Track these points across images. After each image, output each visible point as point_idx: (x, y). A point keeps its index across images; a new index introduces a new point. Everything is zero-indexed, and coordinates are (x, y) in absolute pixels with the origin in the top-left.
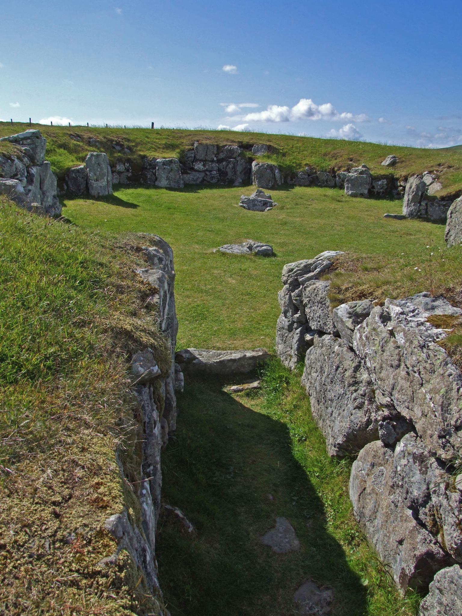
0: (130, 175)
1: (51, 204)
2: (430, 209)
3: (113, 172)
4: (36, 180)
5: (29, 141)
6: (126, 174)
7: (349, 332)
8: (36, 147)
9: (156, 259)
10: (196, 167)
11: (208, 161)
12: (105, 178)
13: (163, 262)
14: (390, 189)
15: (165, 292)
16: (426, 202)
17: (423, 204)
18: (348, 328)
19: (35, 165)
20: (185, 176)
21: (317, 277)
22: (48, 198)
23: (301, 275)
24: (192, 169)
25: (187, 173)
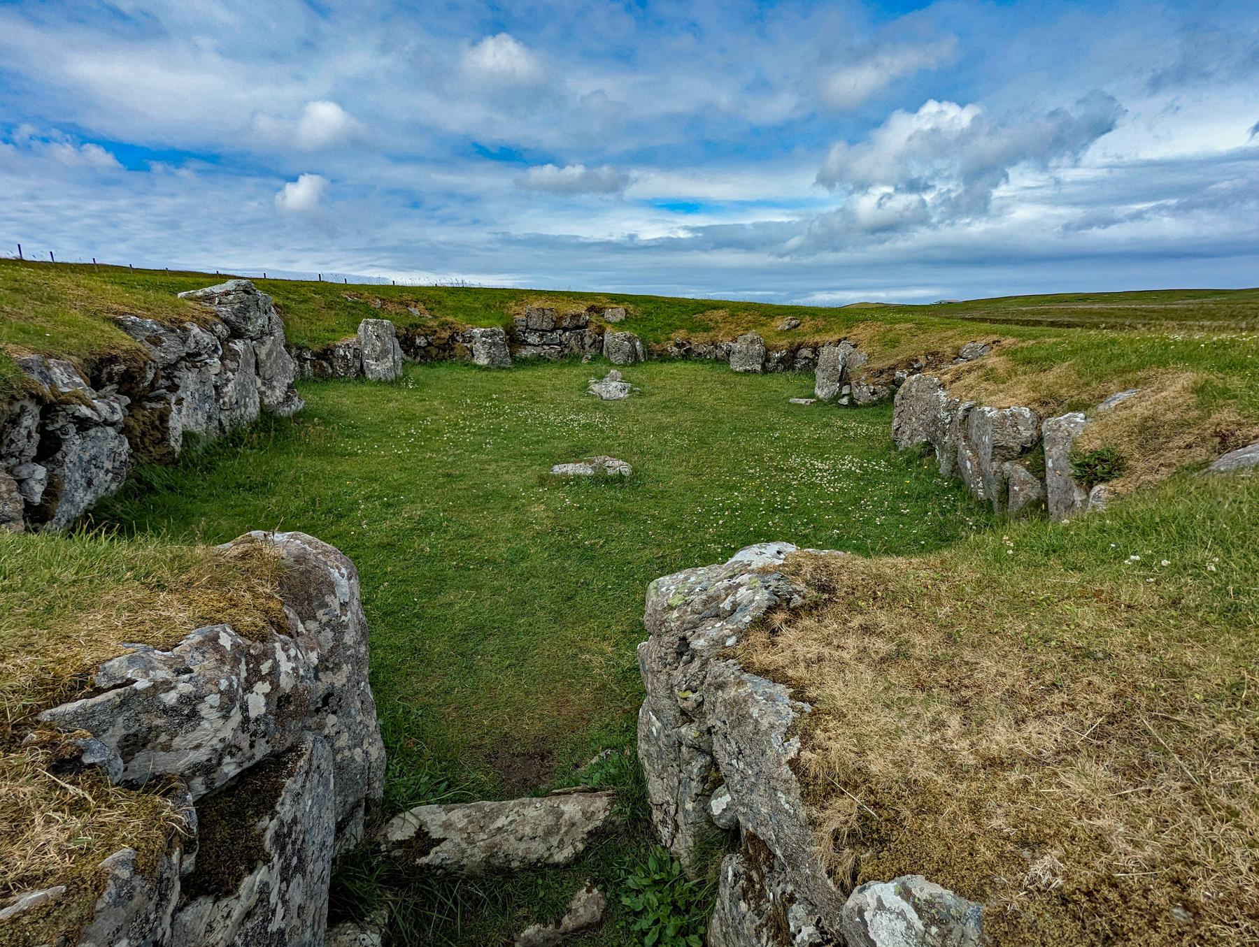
12: (390, 356)
14: (794, 362)
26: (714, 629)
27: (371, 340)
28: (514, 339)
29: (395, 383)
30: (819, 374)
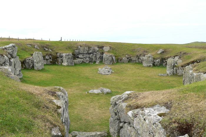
0: (51, 60)
1: (18, 74)
2: (178, 71)
3: (44, 59)
4: (13, 64)
5: (10, 48)
6: (50, 60)
7: (132, 121)
8: (13, 51)
9: (61, 96)
10: (79, 57)
11: (85, 54)
12: (41, 62)
13: (64, 98)
14: (162, 63)
15: (64, 108)
16: (175, 68)
17: (175, 68)
18: (132, 119)
19: (12, 57)
20: (75, 60)
21: (123, 101)
22: (17, 71)
23: (117, 101)
24: (78, 57)
25: (76, 59)
26: (120, 101)
27: (37, 57)
28: (75, 56)
29: (42, 70)
30: (167, 66)
